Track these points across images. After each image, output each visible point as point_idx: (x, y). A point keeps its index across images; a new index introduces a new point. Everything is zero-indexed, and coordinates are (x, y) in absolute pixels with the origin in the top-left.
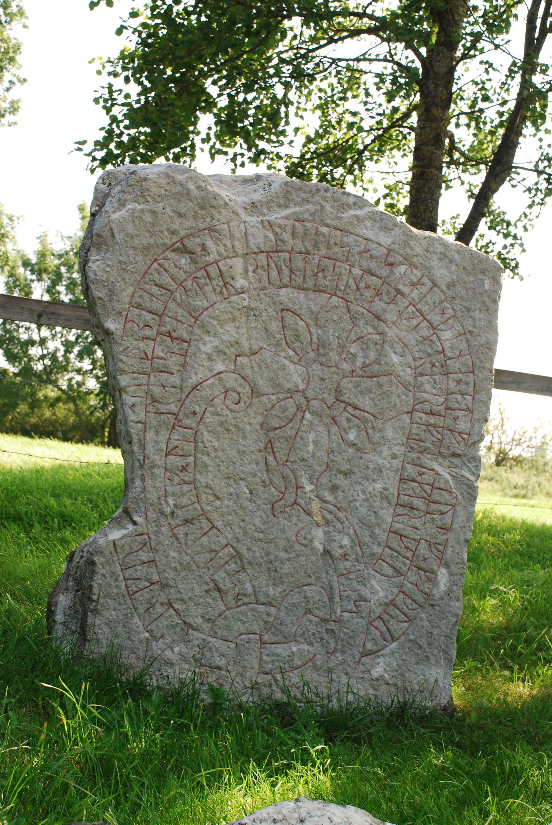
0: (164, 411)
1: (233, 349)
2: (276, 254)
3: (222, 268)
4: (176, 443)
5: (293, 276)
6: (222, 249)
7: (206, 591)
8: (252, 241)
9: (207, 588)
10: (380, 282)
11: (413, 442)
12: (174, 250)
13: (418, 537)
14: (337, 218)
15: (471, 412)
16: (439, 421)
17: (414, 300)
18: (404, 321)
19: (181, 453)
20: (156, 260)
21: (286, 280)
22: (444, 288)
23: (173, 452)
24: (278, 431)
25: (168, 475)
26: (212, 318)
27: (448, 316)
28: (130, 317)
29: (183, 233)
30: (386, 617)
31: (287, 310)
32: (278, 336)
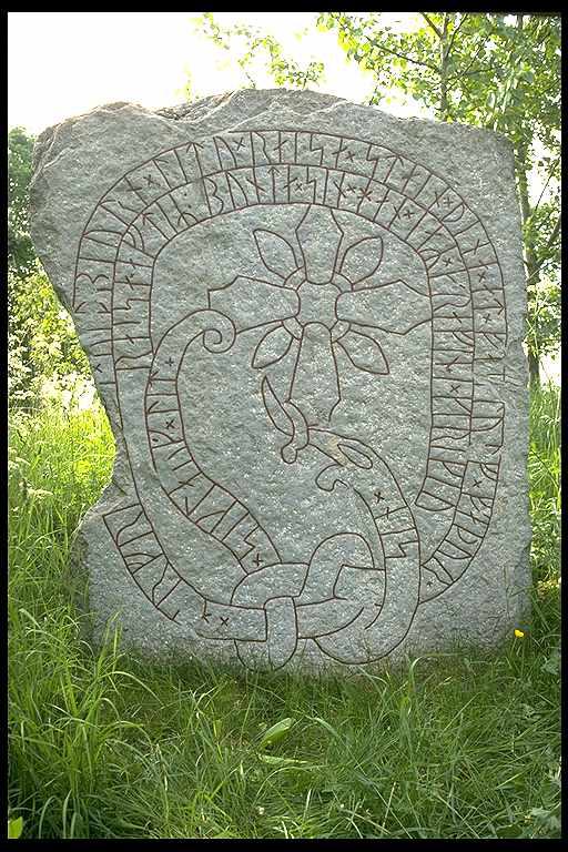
0: (135, 365)
1: (204, 284)
2: (236, 171)
3: (176, 198)
4: (154, 398)
5: (260, 191)
6: (171, 177)
7: (220, 557)
8: (205, 163)
9: (219, 553)
10: (366, 180)
11: (516, 96)
12: (119, 190)
13: (465, 460)
14: (300, 120)
15: (504, 307)
16: (466, 323)
17: (410, 192)
18: (404, 219)
19: (162, 408)
20: (100, 204)
21: (252, 196)
22: (444, 174)
23: (153, 409)
24: (272, 367)
25: (152, 435)
26: (173, 253)
27: (456, 203)
28: (80, 270)
29: (125, 169)
30: (438, 554)
31: (259, 230)
32: (255, 261)
